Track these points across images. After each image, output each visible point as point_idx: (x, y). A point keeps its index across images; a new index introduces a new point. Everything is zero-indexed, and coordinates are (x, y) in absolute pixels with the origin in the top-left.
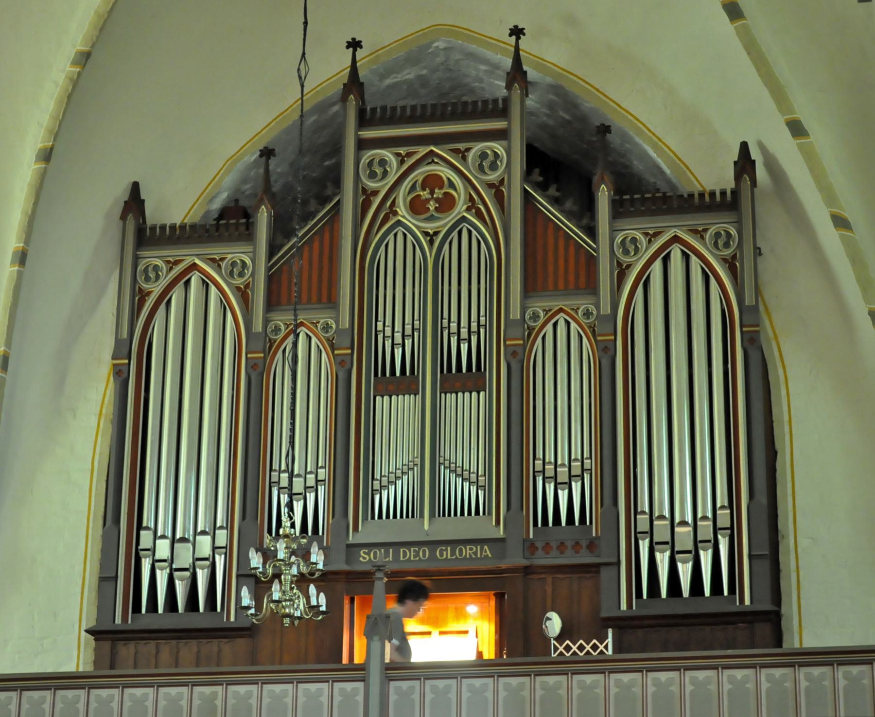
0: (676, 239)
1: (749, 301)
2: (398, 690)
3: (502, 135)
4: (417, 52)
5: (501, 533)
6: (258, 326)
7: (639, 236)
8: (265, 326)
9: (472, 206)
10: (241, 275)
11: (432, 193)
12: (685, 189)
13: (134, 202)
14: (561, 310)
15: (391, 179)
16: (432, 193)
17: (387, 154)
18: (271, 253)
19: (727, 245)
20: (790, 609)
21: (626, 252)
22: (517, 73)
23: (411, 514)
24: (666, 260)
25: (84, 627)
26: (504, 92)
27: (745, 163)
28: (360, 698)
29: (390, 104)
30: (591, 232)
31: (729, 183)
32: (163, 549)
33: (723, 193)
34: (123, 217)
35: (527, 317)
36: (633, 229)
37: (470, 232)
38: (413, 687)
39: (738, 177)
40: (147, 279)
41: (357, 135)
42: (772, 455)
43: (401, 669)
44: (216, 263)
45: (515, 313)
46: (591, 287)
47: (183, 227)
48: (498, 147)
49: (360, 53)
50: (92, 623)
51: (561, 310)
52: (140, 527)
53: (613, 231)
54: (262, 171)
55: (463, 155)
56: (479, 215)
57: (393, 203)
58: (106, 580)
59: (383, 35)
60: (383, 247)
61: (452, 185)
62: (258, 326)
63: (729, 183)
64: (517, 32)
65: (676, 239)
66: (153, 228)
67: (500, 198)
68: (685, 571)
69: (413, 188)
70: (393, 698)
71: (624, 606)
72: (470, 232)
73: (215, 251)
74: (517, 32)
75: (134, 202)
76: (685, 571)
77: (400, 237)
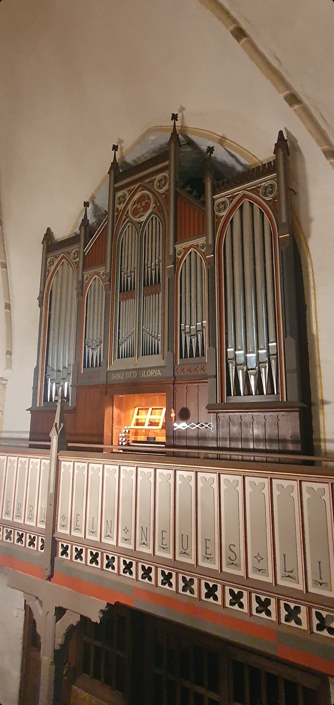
5: (162, 363)
13: (49, 235)
24: (241, 208)
34: (43, 243)
75: (49, 235)
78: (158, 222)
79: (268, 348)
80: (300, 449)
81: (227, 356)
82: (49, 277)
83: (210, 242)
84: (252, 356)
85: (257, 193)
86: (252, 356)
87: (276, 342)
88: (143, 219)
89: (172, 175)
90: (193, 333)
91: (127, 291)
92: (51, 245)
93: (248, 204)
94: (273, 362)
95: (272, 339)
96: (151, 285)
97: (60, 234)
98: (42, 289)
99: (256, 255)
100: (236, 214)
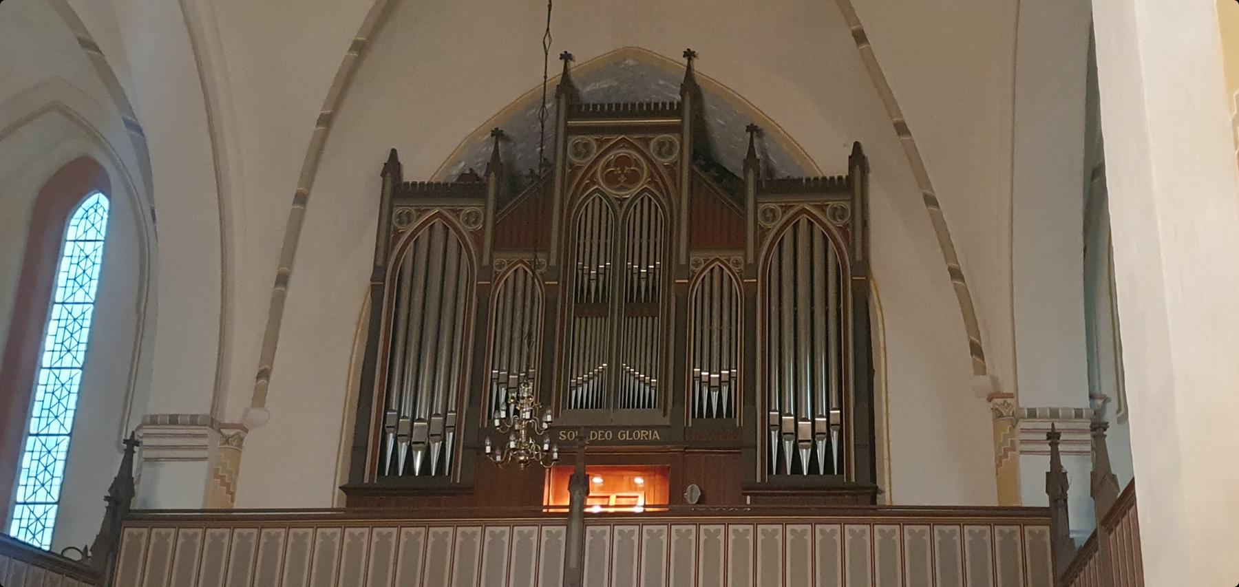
0: (439, 214)
1: (859, 257)
2: (592, 532)
3: (677, 129)
4: (613, 64)
5: (666, 421)
6: (486, 261)
7: (413, 210)
8: (491, 262)
9: (651, 175)
10: (842, 217)
11: (622, 169)
12: (782, 173)
13: (392, 166)
14: (717, 259)
15: (593, 157)
16: (622, 169)
17: (590, 139)
18: (497, 209)
19: (842, 217)
20: (883, 482)
21: (401, 222)
22: (690, 84)
23: (599, 405)
24: (796, 226)
25: (338, 485)
26: (679, 98)
27: (857, 157)
28: (563, 538)
29: (614, 100)
30: (742, 203)
31: (844, 171)
32: (404, 430)
33: (840, 178)
34: (383, 174)
35: (691, 262)
36: (772, 203)
37: (650, 200)
38: (894, 531)
39: (851, 168)
40: (401, 222)
41: (683, 119)
42: (871, 372)
43: (577, 517)
44: (822, 208)
45: (683, 261)
46: (742, 246)
47: (430, 184)
48: (675, 138)
49: (572, 64)
50: (346, 482)
51: (717, 259)
52: (387, 408)
53: (756, 203)
54: (491, 149)
55: (646, 142)
56: (657, 186)
57: (593, 175)
58: (358, 449)
59: (590, 49)
60: (412, 243)
61: (638, 165)
62: (486, 261)
63: (844, 171)
64: (689, 54)
65: (804, 211)
66: (407, 184)
67: (673, 175)
68: (805, 455)
69: (608, 166)
70: (588, 538)
71: (366, 480)
72: (650, 200)
73: (457, 204)
74: (689, 54)
75: (392, 166)
76: (805, 455)
77: (597, 200)
78: (604, 208)
79: (828, 416)
80: (13, 533)
81: (384, 422)
82: (399, 246)
83: (750, 260)
84: (805, 426)
85: (824, 211)
86: (805, 426)
87: (841, 409)
88: (626, 194)
89: (687, 138)
90: (715, 383)
91: (590, 304)
92: (395, 185)
93: (441, 227)
94: (835, 435)
95: (834, 404)
96: (641, 303)
97: (416, 170)
98: (380, 263)
99: (421, 295)
100: (423, 234)
